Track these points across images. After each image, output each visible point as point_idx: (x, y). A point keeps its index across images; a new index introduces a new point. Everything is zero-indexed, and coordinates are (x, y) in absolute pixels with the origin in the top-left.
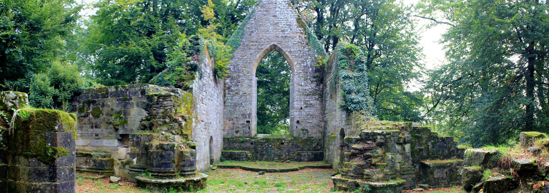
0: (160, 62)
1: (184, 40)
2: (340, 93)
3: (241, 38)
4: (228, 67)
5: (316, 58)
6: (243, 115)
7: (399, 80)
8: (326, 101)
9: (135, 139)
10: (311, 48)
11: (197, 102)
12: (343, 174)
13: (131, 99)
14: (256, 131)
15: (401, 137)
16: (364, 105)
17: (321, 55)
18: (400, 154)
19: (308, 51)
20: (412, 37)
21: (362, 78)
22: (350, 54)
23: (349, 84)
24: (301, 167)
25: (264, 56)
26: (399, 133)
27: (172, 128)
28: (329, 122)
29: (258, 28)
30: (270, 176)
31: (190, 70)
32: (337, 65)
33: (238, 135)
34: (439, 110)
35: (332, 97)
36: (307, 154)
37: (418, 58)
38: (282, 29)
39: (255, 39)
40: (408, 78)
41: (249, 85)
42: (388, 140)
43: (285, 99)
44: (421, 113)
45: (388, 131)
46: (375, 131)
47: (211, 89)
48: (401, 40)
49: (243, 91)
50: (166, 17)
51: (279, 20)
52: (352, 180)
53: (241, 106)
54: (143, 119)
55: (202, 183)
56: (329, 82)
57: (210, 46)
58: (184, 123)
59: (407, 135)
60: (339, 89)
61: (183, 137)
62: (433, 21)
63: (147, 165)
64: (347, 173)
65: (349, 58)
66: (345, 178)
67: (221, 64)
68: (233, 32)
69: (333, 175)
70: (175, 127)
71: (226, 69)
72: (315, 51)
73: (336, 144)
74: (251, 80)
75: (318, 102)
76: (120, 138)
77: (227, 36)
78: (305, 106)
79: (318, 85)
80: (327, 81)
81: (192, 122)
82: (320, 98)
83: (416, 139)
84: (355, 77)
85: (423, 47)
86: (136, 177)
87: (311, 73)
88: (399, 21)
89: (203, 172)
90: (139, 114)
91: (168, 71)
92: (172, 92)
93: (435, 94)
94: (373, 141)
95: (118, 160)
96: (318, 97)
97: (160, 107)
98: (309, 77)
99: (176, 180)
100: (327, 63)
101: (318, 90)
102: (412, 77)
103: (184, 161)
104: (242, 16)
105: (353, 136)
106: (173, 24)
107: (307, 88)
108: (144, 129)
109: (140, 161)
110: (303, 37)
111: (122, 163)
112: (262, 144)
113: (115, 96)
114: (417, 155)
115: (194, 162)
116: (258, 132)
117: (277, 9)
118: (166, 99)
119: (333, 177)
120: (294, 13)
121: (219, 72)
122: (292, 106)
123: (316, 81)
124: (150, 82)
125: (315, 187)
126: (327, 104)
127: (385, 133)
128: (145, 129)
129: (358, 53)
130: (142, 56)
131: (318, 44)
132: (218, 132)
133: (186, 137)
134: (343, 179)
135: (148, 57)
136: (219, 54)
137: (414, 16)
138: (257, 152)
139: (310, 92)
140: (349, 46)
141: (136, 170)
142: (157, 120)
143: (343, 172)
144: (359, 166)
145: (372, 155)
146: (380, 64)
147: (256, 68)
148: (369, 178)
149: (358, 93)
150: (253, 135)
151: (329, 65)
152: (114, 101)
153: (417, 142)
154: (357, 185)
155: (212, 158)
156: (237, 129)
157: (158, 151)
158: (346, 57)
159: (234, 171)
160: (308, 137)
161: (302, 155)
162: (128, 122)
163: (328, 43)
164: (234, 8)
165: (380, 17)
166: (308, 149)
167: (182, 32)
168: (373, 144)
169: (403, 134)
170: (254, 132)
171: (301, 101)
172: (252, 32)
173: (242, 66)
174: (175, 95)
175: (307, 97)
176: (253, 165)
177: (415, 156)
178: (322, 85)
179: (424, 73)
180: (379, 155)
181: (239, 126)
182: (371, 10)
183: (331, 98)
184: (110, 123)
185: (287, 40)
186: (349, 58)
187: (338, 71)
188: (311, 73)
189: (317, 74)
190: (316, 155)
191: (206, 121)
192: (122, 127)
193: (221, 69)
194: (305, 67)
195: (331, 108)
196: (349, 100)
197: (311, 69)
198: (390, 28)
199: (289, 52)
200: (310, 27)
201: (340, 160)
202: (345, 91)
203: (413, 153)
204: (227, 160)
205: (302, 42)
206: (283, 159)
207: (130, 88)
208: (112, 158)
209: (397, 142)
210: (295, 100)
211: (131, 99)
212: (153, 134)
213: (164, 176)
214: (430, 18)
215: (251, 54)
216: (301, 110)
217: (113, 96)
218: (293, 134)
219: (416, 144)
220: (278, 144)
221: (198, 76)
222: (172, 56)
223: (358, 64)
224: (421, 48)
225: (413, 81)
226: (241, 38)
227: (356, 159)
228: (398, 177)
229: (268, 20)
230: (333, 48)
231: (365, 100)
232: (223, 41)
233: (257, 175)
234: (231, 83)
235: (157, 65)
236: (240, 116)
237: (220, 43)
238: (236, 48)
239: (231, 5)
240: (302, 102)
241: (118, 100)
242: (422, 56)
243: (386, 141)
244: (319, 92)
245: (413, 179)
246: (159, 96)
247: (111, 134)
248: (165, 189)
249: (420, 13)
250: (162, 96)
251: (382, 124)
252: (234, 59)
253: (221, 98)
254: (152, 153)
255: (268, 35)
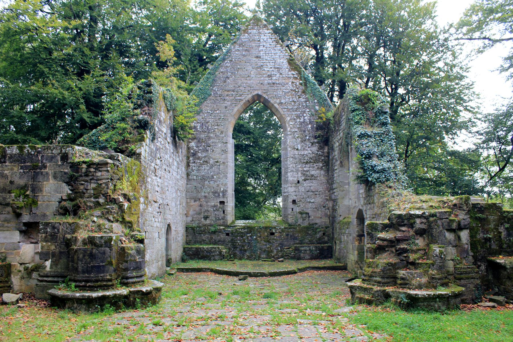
0: (96, 114)
1: (131, 86)
2: (354, 158)
3: (211, 86)
4: (193, 125)
5: (316, 111)
6: (215, 193)
7: (440, 134)
8: (334, 170)
9: (49, 230)
10: (309, 98)
11: (148, 174)
12: (365, 278)
13: (45, 167)
14: (234, 217)
15: (454, 220)
16: (392, 173)
17: (324, 107)
18: (453, 246)
19: (306, 102)
20: (455, 70)
21: (387, 135)
22: (366, 103)
23: (368, 145)
24: (300, 268)
25: (244, 110)
26: (450, 213)
27: (108, 212)
28: (339, 201)
29: (235, 73)
30: (255, 283)
31: (137, 127)
32: (349, 119)
33: (208, 222)
34: (510, 175)
35: (343, 164)
36: (308, 249)
37: (468, 99)
38: (269, 74)
39: (231, 87)
40: (454, 129)
41: (223, 150)
42: (432, 225)
43: (274, 169)
44: (478, 181)
45: (433, 211)
46: (412, 212)
47: (168, 156)
48: (438, 77)
49: (214, 159)
50: (107, 53)
51: (265, 61)
52: (379, 288)
53: (212, 180)
54: (64, 198)
55: (154, 296)
56: (337, 144)
57: (168, 95)
58: (126, 205)
59: (462, 216)
60: (354, 152)
61: (125, 226)
62: (487, 41)
63: (69, 270)
64: (371, 276)
65: (365, 108)
66: (368, 284)
67: (183, 121)
68: (200, 78)
69: (350, 280)
70: (113, 211)
71: (191, 128)
72: (316, 101)
73: (352, 232)
74: (226, 143)
75: (322, 172)
76: (24, 228)
77: (192, 83)
78: (303, 178)
79: (321, 148)
80: (334, 143)
81: (139, 203)
82: (324, 166)
83: (478, 222)
84: (375, 134)
85: (473, 82)
86: (50, 291)
87: (311, 131)
88: (434, 51)
89: (155, 279)
90: (56, 191)
91: (106, 128)
92: (110, 158)
93: (500, 150)
94: (409, 228)
95: (19, 265)
96: (321, 165)
97: (91, 180)
98: (308, 138)
99: (114, 292)
100: (334, 117)
101: (322, 156)
102: (460, 128)
103: (127, 262)
104: (213, 57)
105: (376, 220)
106: (117, 63)
107: (306, 152)
108: (64, 214)
109: (57, 265)
110: (298, 83)
111: (26, 269)
112: (242, 235)
113: (18, 161)
114: (481, 247)
115: (142, 264)
116: (237, 218)
117: (261, 48)
118: (101, 169)
119: (349, 284)
120: (284, 52)
121: (180, 132)
122: (285, 180)
123: (317, 143)
124: (78, 142)
125: (322, 298)
126: (335, 175)
127: (427, 214)
128: (67, 214)
129: (378, 100)
130: (68, 103)
131: (319, 92)
132: (179, 217)
133: (130, 225)
134: (365, 286)
135: (77, 106)
136: (179, 107)
137: (455, 40)
138: (235, 247)
139: (310, 158)
140: (364, 92)
141: (50, 279)
142: (85, 199)
143: (364, 275)
144: (389, 266)
145: (409, 248)
146: (409, 114)
147: (233, 126)
148: (406, 284)
149: (382, 157)
150: (229, 222)
151: (337, 119)
152: (16, 169)
153: (480, 227)
154: (387, 296)
155: (169, 257)
156: (206, 214)
157: (86, 247)
158: (361, 107)
159: (202, 277)
160: (309, 224)
161: (301, 251)
162: (39, 203)
163: (332, 90)
164: (202, 46)
165: (404, 49)
166: (310, 241)
167: (128, 75)
168: (409, 231)
169: (456, 216)
170: (230, 218)
171: (297, 171)
172: (228, 78)
173: (213, 124)
174: (114, 164)
175: (307, 166)
176: (230, 266)
177: (477, 249)
178: (326, 148)
179: (479, 119)
180: (421, 248)
181: (209, 209)
182: (390, 41)
183: (341, 167)
184: (8, 205)
185: (276, 88)
186: (365, 108)
187: (350, 127)
188: (311, 131)
189: (319, 132)
190: (322, 250)
191: (161, 202)
192: (28, 211)
193: (183, 127)
194: (301, 123)
195: (342, 181)
196: (369, 168)
197: (310, 126)
198: (420, 62)
199: (278, 104)
200: (306, 69)
201: (358, 257)
202: (362, 155)
203: (473, 244)
204: (192, 259)
205: (297, 90)
206: (273, 257)
207: (45, 149)
208: (8, 262)
209: (447, 227)
210: (289, 171)
211: (45, 167)
212: (78, 221)
213: (95, 287)
214: (482, 37)
215: (226, 107)
216: (298, 185)
217: (14, 161)
218: (287, 220)
219: (478, 230)
220: (266, 234)
221: (149, 136)
222: (112, 107)
223: (379, 116)
224: (471, 83)
225: (463, 134)
226: (211, 86)
227: (385, 255)
228: (451, 283)
229: (249, 61)
230: (341, 96)
231: (392, 166)
232: (186, 90)
233: (236, 282)
234: (197, 147)
235: (91, 118)
236: (211, 194)
237: (182, 92)
238: (205, 99)
239: (198, 43)
240: (299, 173)
241: (22, 168)
242: (473, 95)
243: (429, 226)
244: (323, 158)
245: (476, 286)
246: (90, 164)
247: (8, 223)
248: (97, 307)
249: (464, 34)
250: (93, 164)
251: (421, 200)
252: (201, 114)
253: (183, 169)
254: (76, 251)
255: (249, 82)
